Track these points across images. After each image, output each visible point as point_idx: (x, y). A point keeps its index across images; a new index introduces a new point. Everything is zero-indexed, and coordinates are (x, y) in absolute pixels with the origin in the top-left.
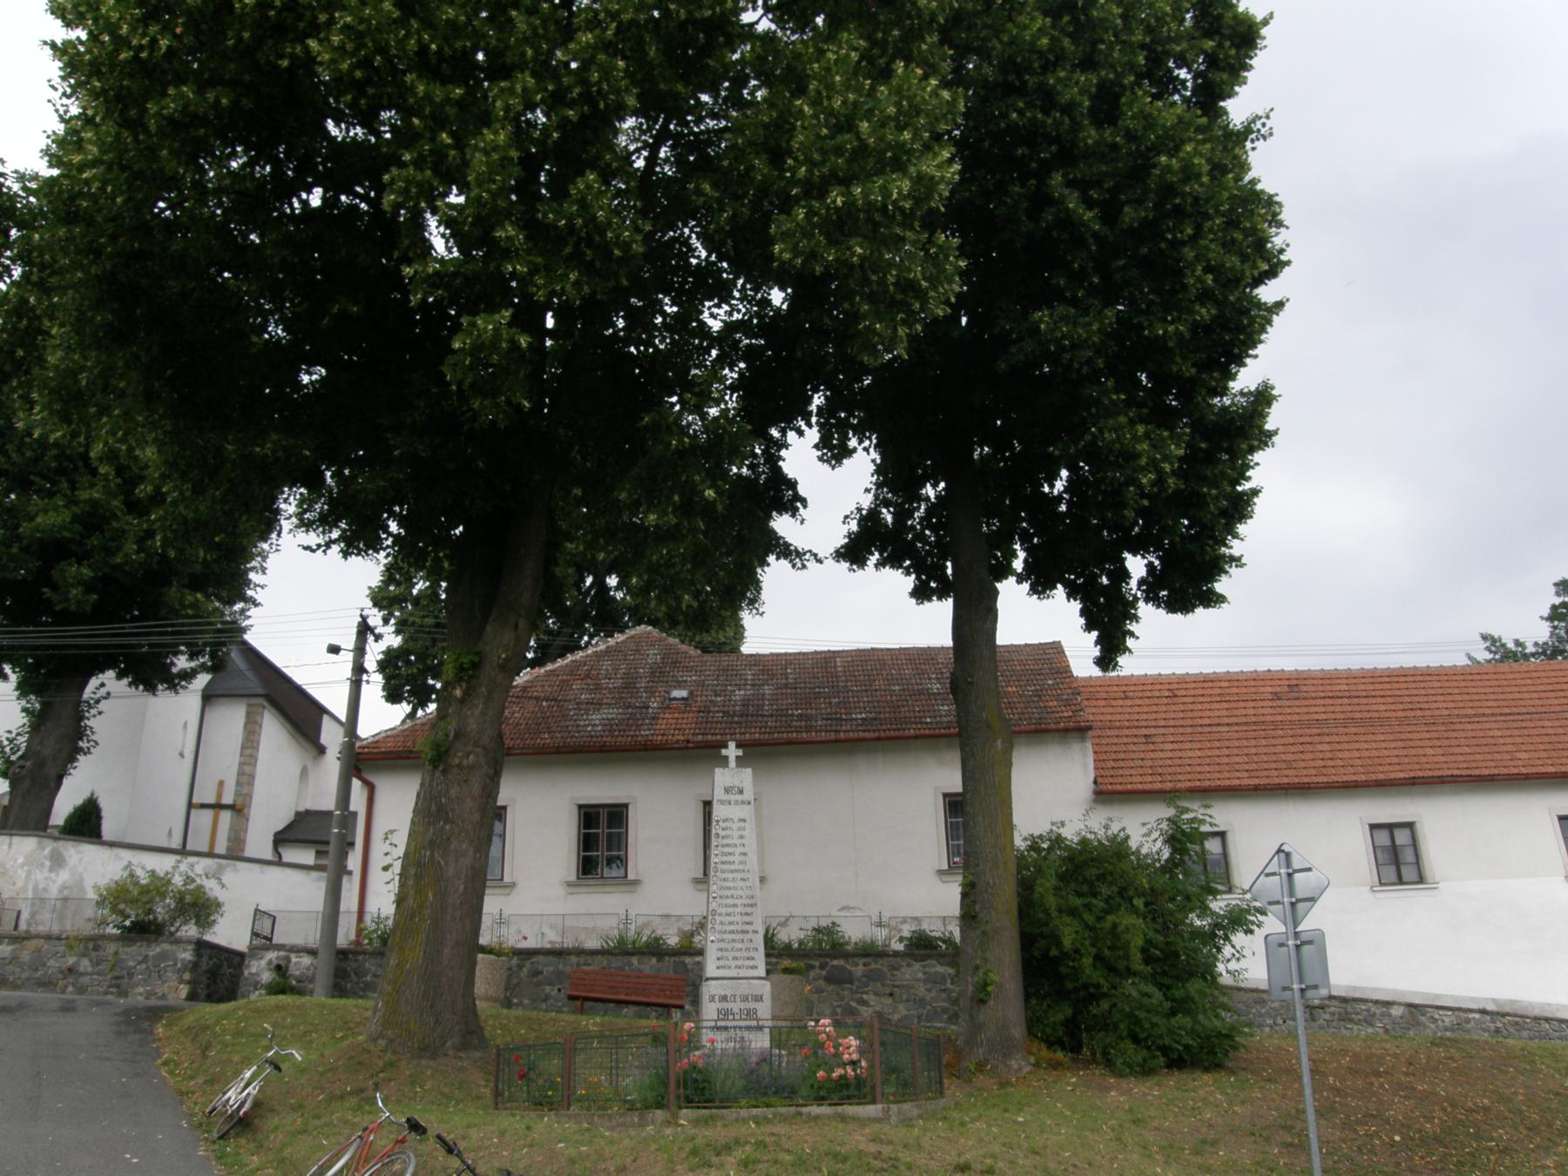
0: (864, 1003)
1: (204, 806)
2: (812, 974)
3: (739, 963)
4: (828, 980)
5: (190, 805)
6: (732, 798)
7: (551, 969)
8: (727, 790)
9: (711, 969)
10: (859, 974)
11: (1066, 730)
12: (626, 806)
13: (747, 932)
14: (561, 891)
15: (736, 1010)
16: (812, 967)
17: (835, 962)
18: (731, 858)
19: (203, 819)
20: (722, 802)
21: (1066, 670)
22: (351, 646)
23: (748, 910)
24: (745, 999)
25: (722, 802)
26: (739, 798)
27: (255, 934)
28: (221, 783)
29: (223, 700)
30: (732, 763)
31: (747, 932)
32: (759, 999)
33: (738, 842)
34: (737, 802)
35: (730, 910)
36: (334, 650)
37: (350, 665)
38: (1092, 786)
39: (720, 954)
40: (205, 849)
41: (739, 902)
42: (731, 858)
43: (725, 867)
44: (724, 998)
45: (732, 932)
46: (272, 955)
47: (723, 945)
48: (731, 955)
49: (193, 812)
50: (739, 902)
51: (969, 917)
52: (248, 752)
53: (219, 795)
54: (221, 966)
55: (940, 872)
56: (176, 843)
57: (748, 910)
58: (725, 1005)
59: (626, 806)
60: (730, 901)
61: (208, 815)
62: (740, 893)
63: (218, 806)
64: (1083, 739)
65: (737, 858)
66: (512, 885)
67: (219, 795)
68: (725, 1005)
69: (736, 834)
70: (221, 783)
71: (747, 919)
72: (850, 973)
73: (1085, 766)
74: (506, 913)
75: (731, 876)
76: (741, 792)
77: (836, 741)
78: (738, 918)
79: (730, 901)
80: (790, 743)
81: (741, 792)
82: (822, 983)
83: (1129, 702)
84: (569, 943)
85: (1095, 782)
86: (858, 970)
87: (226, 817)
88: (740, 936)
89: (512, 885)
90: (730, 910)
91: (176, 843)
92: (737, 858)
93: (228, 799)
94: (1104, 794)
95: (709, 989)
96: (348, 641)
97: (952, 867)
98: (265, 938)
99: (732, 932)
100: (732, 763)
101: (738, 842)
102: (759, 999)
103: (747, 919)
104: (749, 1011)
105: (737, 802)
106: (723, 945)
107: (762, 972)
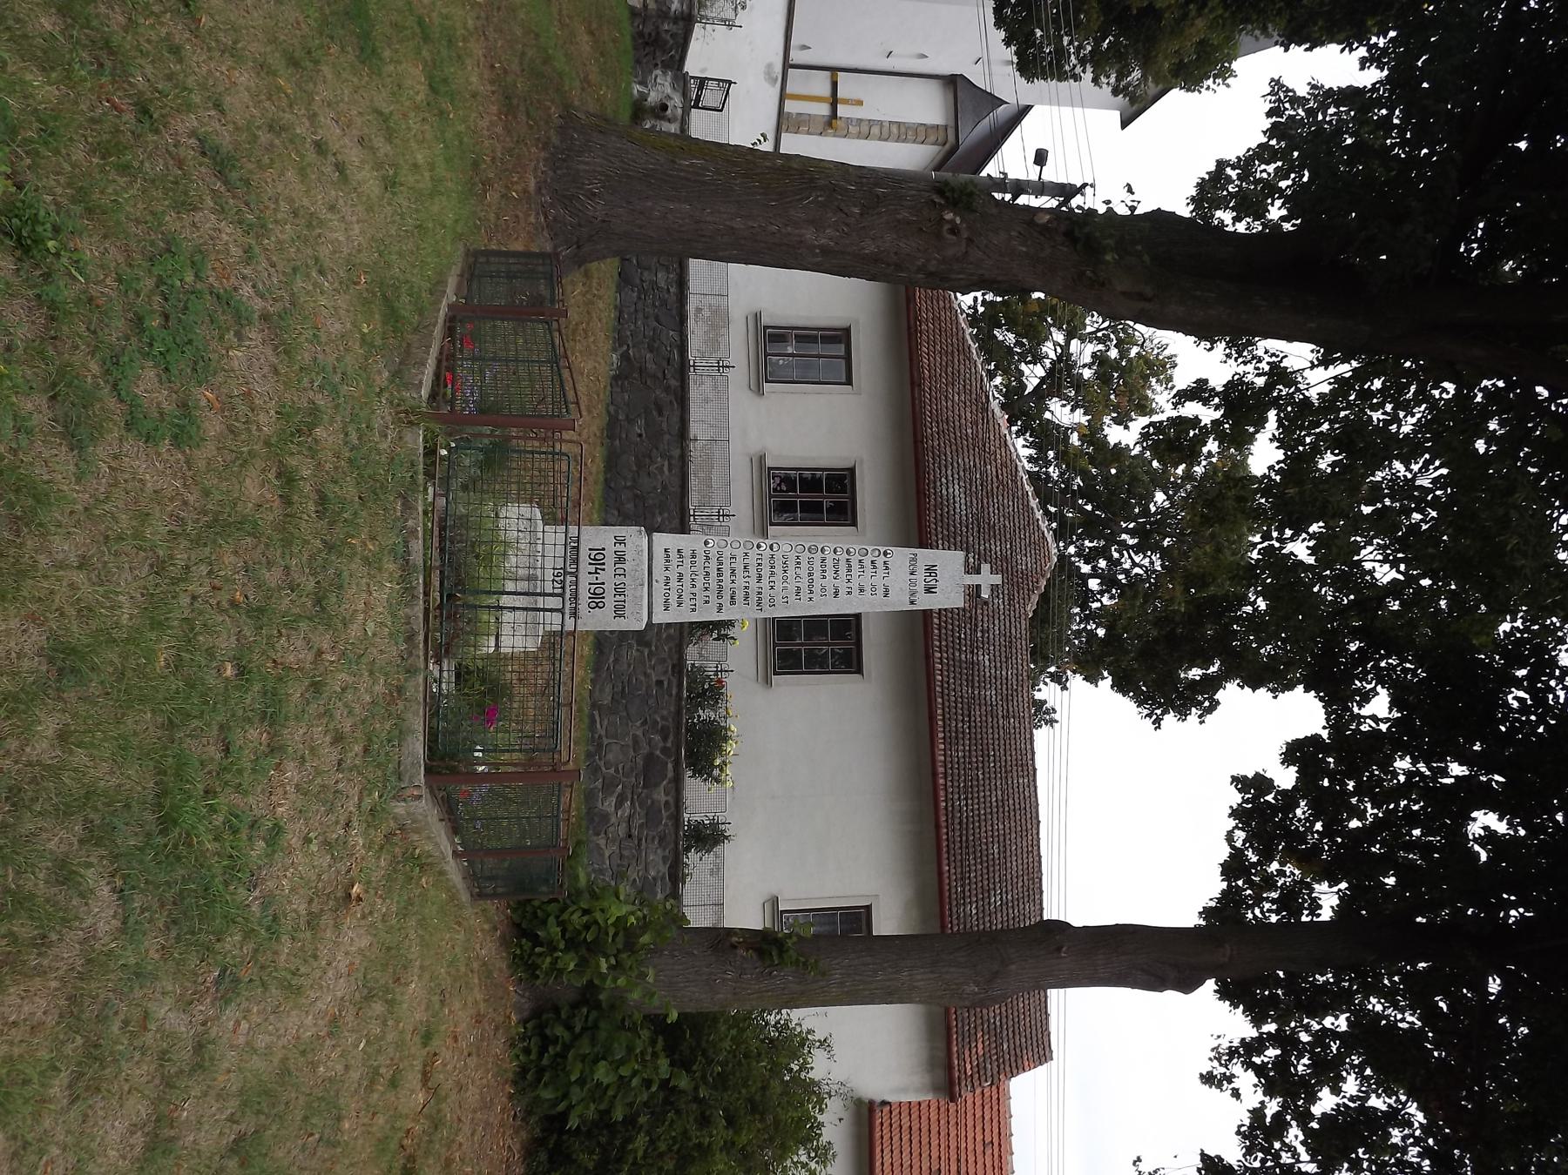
0: (619, 805)
1: (834, 85)
2: (657, 738)
3: (674, 584)
4: (650, 759)
5: (834, 70)
6: (921, 575)
7: (664, 426)
8: (931, 570)
9: (663, 540)
10: (655, 796)
11: (950, 1067)
12: (854, 524)
13: (720, 596)
14: (755, 448)
15: (602, 577)
16: (665, 739)
17: (670, 766)
18: (830, 574)
19: (819, 84)
20: (914, 559)
21: (1017, 1068)
22: (1045, 177)
23: (753, 598)
24: (619, 591)
25: (914, 559)
26: (920, 587)
27: (702, 82)
28: (860, 103)
29: (951, 96)
30: (973, 580)
31: (720, 596)
32: (619, 612)
33: (855, 585)
34: (913, 583)
35: (753, 571)
36: (1041, 158)
37: (1023, 177)
38: (878, 1099)
39: (687, 553)
40: (789, 90)
41: (765, 582)
42: (830, 574)
43: (817, 564)
44: (621, 559)
45: (720, 572)
46: (677, 100)
47: (700, 559)
48: (686, 570)
49: (828, 73)
50: (765, 582)
51: (721, 940)
52: (894, 129)
53: (846, 102)
54: (664, 52)
55: (775, 901)
56: (796, 56)
57: (753, 598)
58: (610, 560)
59: (854, 524)
60: (766, 571)
61: (826, 91)
62: (779, 586)
63: (834, 102)
64: (936, 1089)
65: (829, 581)
66: (759, 392)
67: (846, 102)
68: (610, 560)
69: (867, 581)
70: (860, 103)
71: (740, 596)
72: (657, 785)
73: (905, 1090)
74: (730, 373)
75: (804, 572)
76: (929, 590)
77: (935, 774)
78: (740, 581)
79: (766, 571)
80: (932, 718)
81: (929, 590)
82: (645, 750)
83: (979, 1149)
84: (696, 451)
85: (884, 1103)
86: (660, 796)
87: (823, 110)
88: (714, 585)
89: (759, 392)
90: (753, 571)
91: (796, 56)
92: (829, 581)
93: (842, 111)
94: (866, 1114)
95: (635, 537)
96: (1051, 174)
97: (778, 914)
98: (699, 97)
99: (720, 572)
100: (973, 580)
101: (855, 585)
102: (619, 612)
103: (740, 596)
104: (601, 596)
105: (913, 583)
106: (700, 559)
107: (660, 617)
